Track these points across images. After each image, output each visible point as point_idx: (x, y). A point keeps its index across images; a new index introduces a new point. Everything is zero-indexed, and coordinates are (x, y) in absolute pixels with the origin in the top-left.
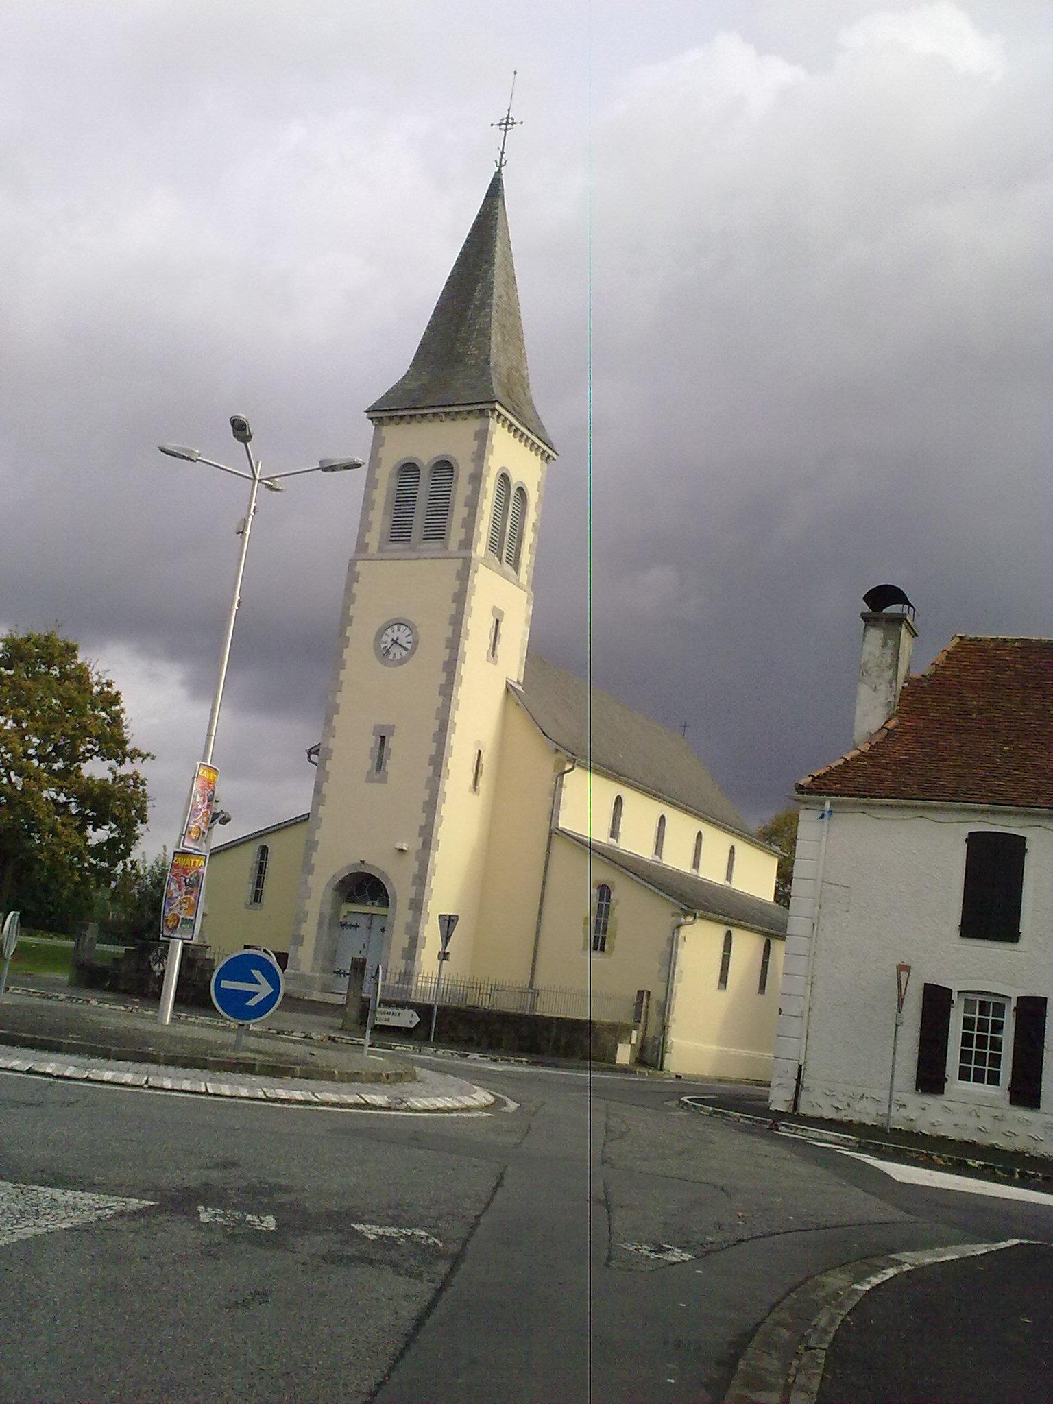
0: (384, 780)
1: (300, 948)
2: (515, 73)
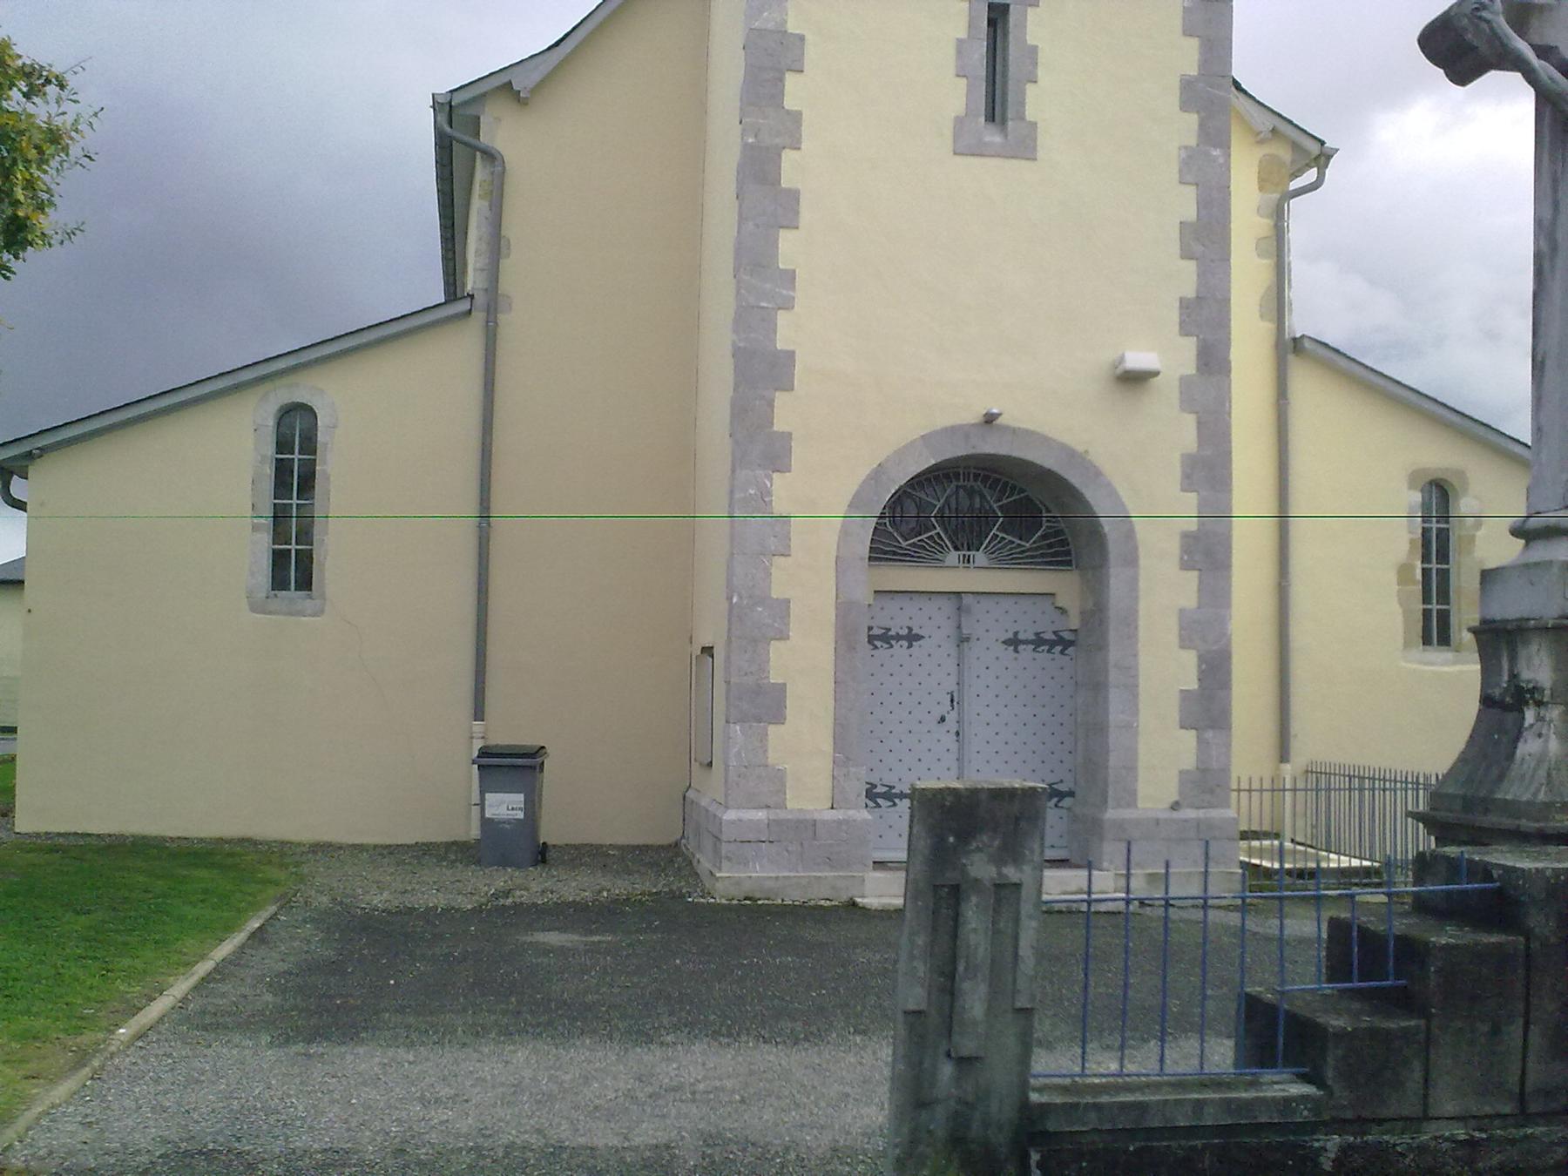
0: (1025, 149)
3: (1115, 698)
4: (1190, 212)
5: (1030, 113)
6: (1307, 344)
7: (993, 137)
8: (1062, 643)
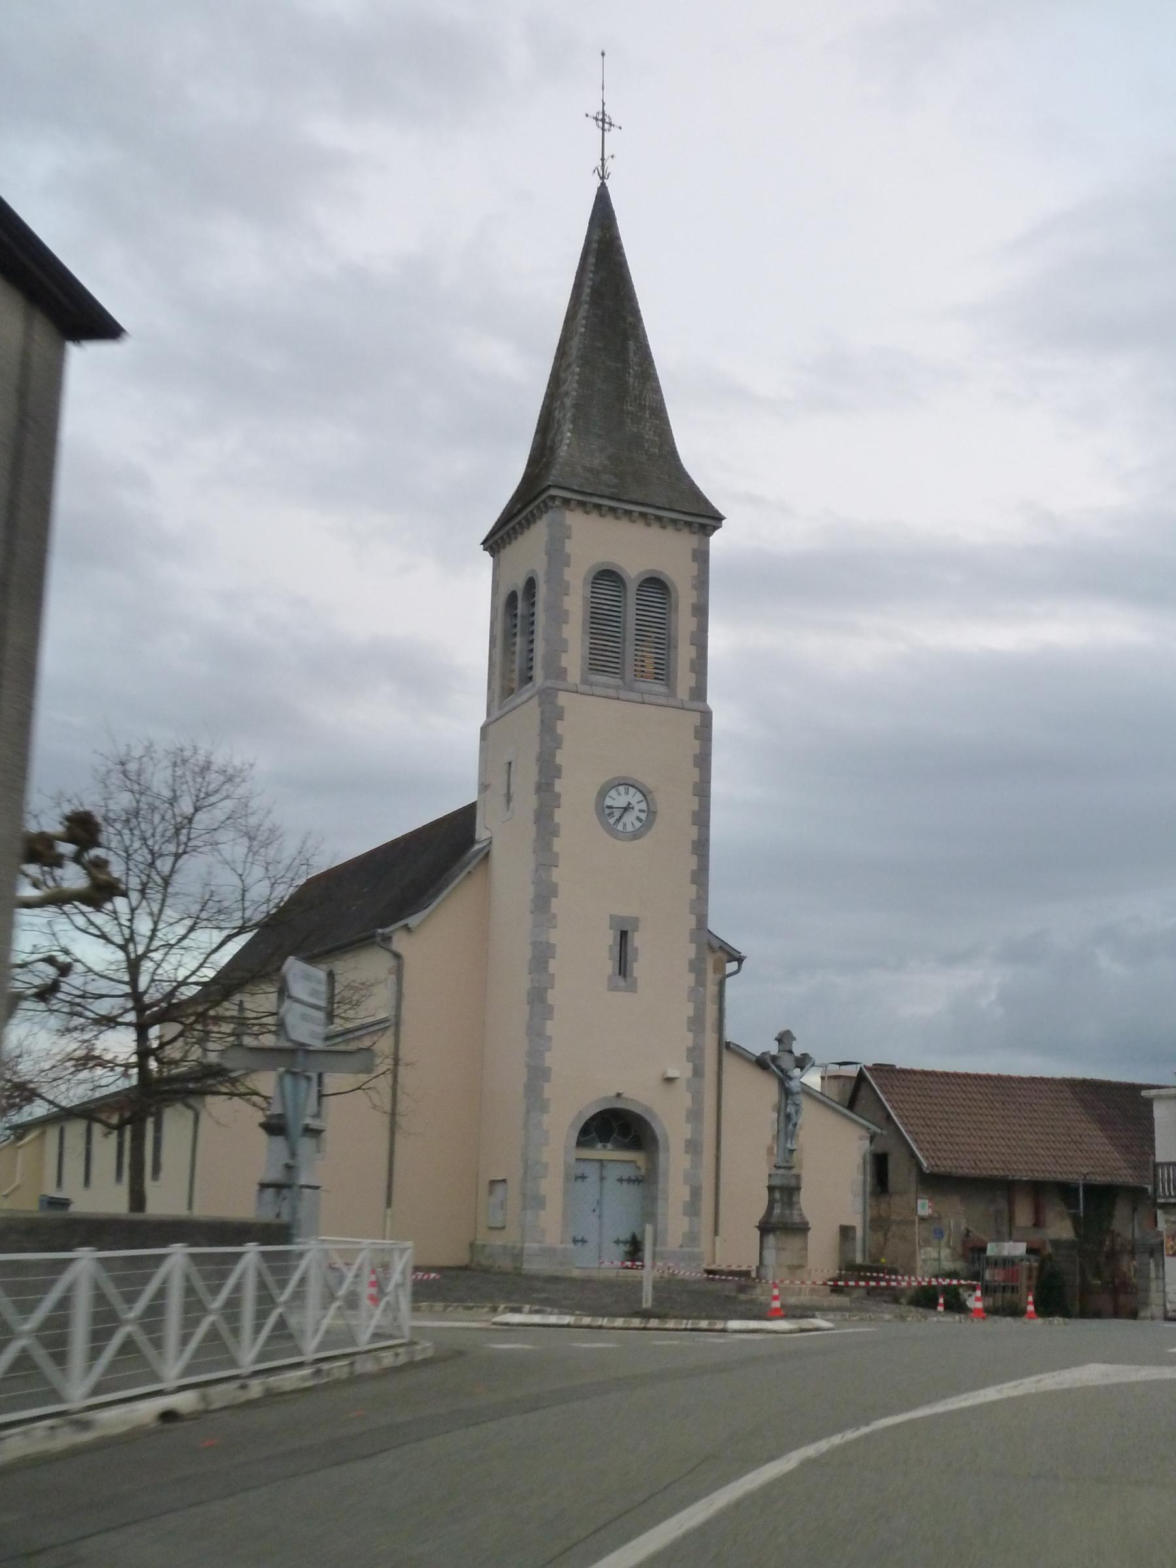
0: (632, 988)
1: (542, 1213)
2: (603, 54)
3: (660, 1203)
4: (691, 1013)
5: (635, 974)
6: (731, 1046)
7: (621, 983)
8: (637, 1181)
